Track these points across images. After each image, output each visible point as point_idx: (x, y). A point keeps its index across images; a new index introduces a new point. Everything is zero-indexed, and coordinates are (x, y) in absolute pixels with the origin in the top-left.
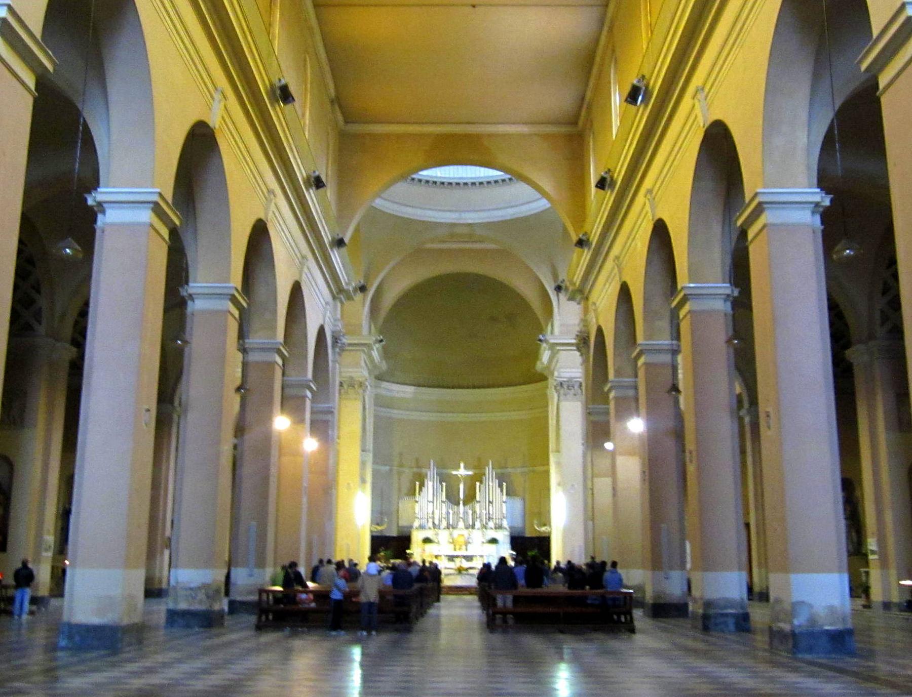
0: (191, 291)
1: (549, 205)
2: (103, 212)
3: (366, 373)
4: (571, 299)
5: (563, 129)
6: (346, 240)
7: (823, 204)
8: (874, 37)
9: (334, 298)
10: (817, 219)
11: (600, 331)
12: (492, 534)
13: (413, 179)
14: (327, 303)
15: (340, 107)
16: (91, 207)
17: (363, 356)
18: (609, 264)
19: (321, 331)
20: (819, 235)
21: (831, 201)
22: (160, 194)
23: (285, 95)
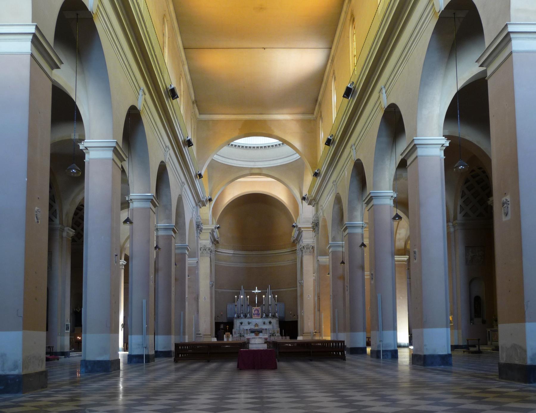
0: (131, 197)
2: (88, 153)
4: (310, 204)
6: (203, 174)
9: (197, 205)
10: (442, 154)
13: (232, 145)
14: (194, 207)
15: (197, 105)
16: (82, 150)
18: (330, 184)
21: (450, 144)
23: (173, 94)
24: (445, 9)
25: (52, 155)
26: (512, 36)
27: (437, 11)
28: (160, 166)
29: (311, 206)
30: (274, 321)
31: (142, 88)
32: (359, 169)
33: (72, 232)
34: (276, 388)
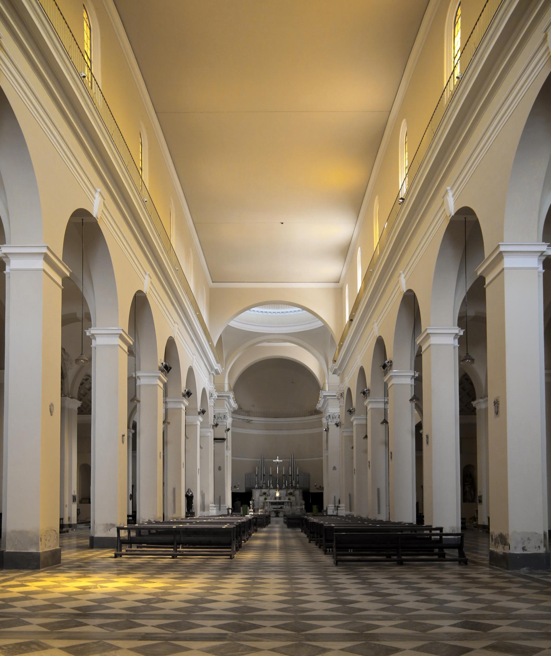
1: (323, 324)
2: (95, 339)
3: (227, 411)
5: (332, 285)
7: (460, 334)
8: (486, 258)
11: (349, 390)
12: (291, 491)
16: (89, 336)
17: (226, 402)
21: (464, 333)
22: (123, 330)
25: (62, 316)
26: (504, 254)
27: (448, 215)
28: (168, 340)
29: (335, 376)
30: (297, 492)
31: (148, 273)
32: (410, 302)
33: (78, 404)
34: (304, 569)
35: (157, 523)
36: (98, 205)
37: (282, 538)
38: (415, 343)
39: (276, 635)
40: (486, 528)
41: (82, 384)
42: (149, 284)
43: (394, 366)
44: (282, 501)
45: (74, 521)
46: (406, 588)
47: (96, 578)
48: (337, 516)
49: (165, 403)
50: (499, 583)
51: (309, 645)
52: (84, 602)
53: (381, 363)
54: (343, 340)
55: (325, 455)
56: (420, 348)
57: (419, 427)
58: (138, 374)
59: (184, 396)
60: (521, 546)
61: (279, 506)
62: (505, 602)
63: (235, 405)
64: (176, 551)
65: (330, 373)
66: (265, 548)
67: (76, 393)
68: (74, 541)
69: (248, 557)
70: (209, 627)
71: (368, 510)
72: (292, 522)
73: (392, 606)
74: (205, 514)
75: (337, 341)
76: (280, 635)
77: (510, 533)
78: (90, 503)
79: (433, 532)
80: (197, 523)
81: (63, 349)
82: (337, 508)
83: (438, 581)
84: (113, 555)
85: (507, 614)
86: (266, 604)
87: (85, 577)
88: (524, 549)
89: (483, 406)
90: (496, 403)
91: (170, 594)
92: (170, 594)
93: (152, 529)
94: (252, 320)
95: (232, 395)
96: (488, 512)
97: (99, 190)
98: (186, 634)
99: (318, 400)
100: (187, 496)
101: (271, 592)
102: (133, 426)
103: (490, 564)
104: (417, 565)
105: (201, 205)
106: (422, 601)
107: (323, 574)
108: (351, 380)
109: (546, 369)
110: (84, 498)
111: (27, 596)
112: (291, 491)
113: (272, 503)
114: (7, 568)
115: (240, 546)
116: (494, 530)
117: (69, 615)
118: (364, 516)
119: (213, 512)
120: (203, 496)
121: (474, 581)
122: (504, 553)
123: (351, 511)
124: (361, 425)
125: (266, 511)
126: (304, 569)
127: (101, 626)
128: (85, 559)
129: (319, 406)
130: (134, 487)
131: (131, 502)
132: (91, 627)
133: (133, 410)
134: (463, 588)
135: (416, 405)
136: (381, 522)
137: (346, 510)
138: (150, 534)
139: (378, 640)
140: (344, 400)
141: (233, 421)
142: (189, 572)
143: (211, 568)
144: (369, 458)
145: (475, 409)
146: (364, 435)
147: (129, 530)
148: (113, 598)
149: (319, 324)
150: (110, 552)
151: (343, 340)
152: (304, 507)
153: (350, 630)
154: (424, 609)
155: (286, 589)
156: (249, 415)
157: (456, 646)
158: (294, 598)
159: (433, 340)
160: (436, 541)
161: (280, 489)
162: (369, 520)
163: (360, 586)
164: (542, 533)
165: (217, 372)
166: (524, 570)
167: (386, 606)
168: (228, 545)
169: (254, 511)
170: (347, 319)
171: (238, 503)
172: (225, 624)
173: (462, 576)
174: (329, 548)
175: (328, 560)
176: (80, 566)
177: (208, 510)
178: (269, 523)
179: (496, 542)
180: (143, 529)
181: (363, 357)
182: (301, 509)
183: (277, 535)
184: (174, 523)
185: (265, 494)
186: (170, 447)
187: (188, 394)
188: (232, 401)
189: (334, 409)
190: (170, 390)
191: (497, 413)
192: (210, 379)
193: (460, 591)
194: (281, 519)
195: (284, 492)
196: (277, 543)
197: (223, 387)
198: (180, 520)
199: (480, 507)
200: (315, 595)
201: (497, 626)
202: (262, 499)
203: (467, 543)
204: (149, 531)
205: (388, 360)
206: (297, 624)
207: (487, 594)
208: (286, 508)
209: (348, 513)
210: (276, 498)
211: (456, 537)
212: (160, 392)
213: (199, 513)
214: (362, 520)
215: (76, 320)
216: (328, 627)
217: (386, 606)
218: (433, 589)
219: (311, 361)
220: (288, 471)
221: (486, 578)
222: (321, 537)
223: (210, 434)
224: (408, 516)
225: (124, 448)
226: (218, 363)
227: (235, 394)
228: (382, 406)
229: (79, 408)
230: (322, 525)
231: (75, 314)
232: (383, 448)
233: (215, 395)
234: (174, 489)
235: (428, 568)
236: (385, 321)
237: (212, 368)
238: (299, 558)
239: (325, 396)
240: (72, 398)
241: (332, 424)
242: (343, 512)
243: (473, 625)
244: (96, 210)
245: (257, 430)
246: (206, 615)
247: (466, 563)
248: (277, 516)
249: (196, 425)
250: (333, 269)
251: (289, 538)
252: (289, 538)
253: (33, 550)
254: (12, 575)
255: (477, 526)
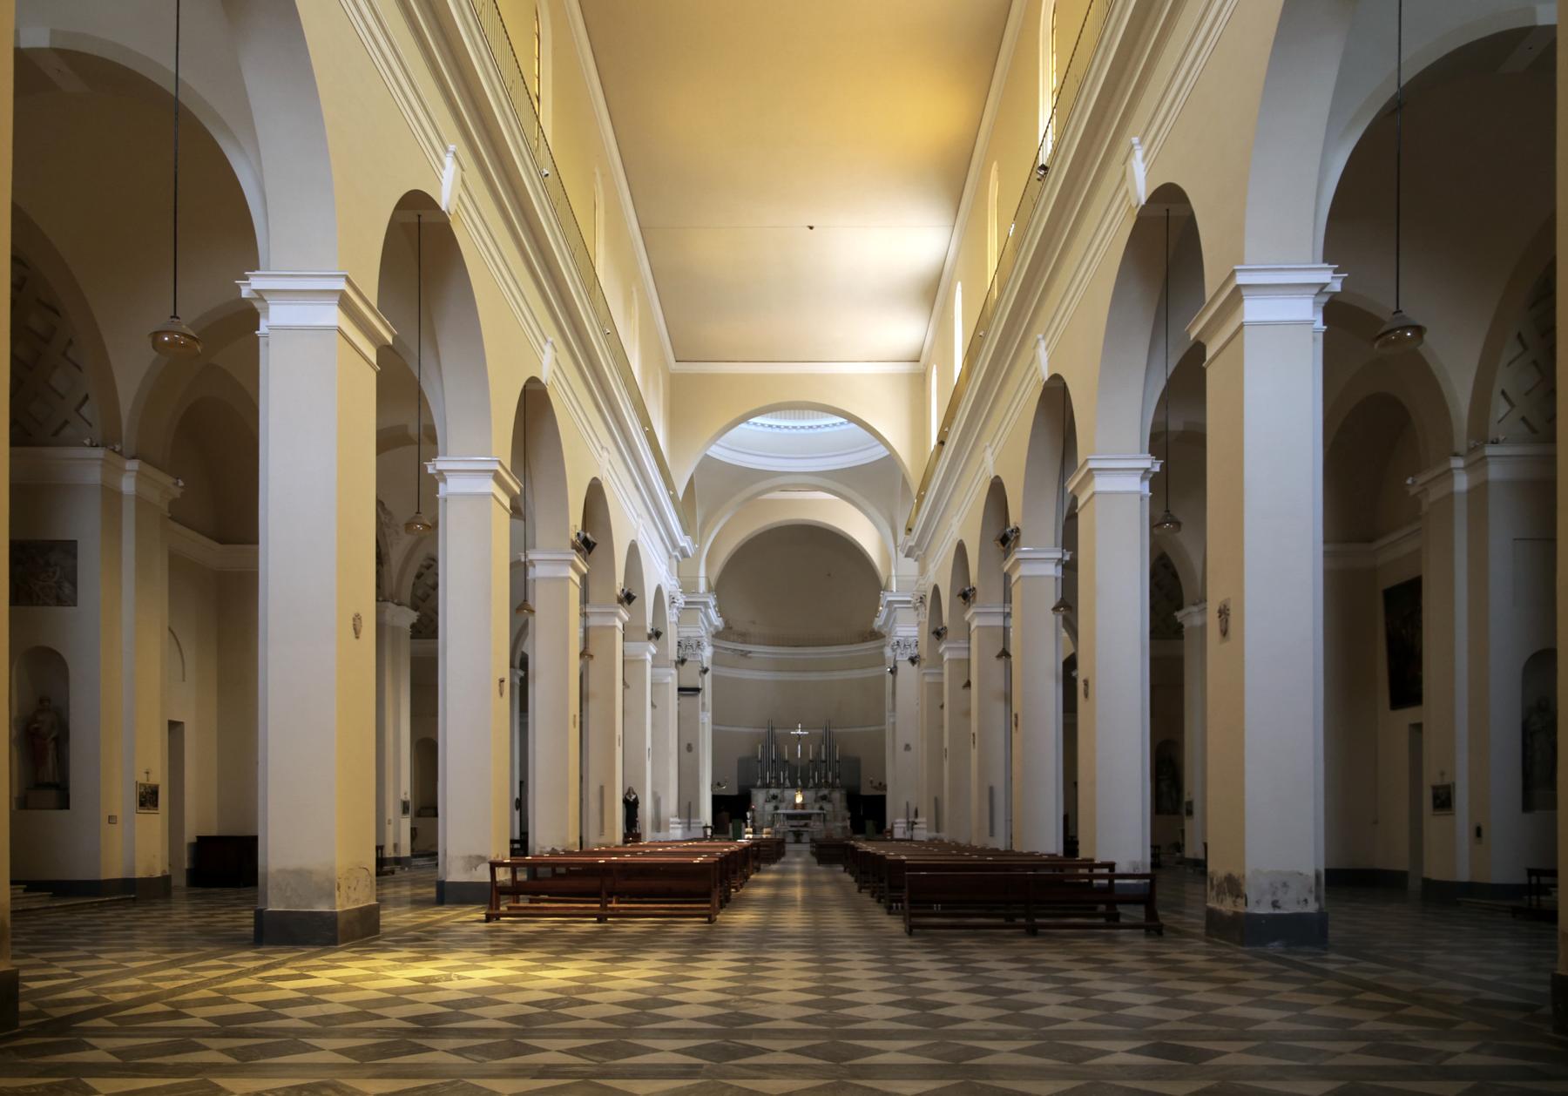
2: (445, 481)
5: (905, 368)
10: (1145, 489)
11: (936, 589)
12: (825, 792)
16: (431, 475)
19: (659, 590)
20: (1147, 501)
21: (1343, 284)
24: (1148, 202)
25: (379, 433)
28: (590, 486)
29: (910, 560)
30: (837, 795)
33: (413, 616)
34: (848, 942)
35: (569, 853)
36: (451, 183)
37: (807, 884)
38: (1064, 489)
39: (794, 1066)
40: (1200, 865)
41: (419, 576)
42: (550, 363)
43: (1022, 539)
44: (808, 811)
45: (406, 852)
46: (1042, 980)
47: (449, 960)
48: (911, 840)
49: (584, 615)
50: (1226, 971)
51: (857, 1086)
52: (425, 1005)
53: (995, 533)
54: (924, 486)
55: (889, 720)
56: (1075, 499)
57: (1070, 664)
58: (531, 556)
59: (620, 601)
60: (1269, 898)
61: (802, 822)
62: (1234, 1007)
63: (718, 622)
64: (607, 909)
65: (901, 555)
66: (776, 903)
67: (406, 595)
68: (406, 891)
69: (743, 918)
70: (667, 1052)
71: (970, 830)
72: (827, 852)
73: (1017, 1014)
74: (661, 836)
75: (915, 486)
76: (802, 1066)
77: (1248, 873)
78: (436, 815)
79: (1096, 871)
80: (645, 854)
81: (380, 503)
82: (911, 825)
83: (1104, 965)
84: (483, 917)
85: (1239, 1030)
86: (771, 1007)
87: (428, 959)
88: (1275, 904)
89: (1197, 621)
90: (1223, 613)
91: (592, 990)
92: (592, 990)
93: (559, 865)
94: (753, 443)
95: (712, 601)
96: (1204, 832)
97: (452, 147)
98: (624, 1066)
99: (877, 610)
100: (626, 801)
101: (787, 984)
102: (521, 663)
103: (1208, 934)
104: (1065, 936)
105: (660, 189)
106: (1073, 1004)
107: (885, 955)
108: (940, 570)
109: (1325, 542)
110: (425, 807)
111: (311, 997)
112: (825, 792)
113: (789, 817)
114: (271, 943)
115: (728, 899)
116: (1217, 867)
117: (397, 1030)
118: (963, 841)
119: (676, 832)
120: (657, 802)
121: (1175, 967)
122: (1236, 913)
123: (938, 831)
124: (959, 661)
125: (777, 832)
126: (848, 942)
127: (458, 1052)
128: (429, 924)
129: (878, 622)
130: (523, 784)
131: (517, 813)
132: (440, 1054)
133: (520, 633)
134: (1154, 980)
135: (1065, 619)
136: (995, 852)
137: (929, 830)
138: (555, 875)
139: (988, 1078)
140: (926, 611)
141: (715, 654)
142: (632, 948)
143: (672, 941)
144: (974, 727)
145: (1182, 626)
146: (964, 682)
147: (514, 867)
148: (482, 998)
149: (881, 452)
150: (476, 911)
151: (924, 486)
152: (848, 823)
153: (934, 1057)
154: (1076, 1019)
155: (815, 980)
156: (744, 642)
157: (1138, 1090)
158: (828, 997)
159: (1100, 484)
160: (1101, 889)
161: (804, 788)
162: (973, 850)
163: (955, 975)
164: (1312, 874)
165: (684, 554)
166: (1275, 947)
167: (1005, 1012)
168: (704, 896)
169: (754, 832)
170: (934, 441)
171: (725, 815)
172: (697, 1047)
173: (1152, 957)
174: (897, 901)
175: (895, 925)
176: (418, 939)
177: (667, 829)
178: (783, 854)
179: (1220, 893)
180: (541, 865)
181: (963, 521)
182: (844, 828)
183: (798, 877)
184: (601, 854)
185: (774, 797)
186: (593, 706)
187: (628, 598)
188: (712, 613)
189: (908, 629)
190: (594, 589)
191: (1224, 632)
192: (670, 567)
193: (1147, 986)
194: (806, 848)
195: (811, 794)
196: (798, 892)
197: (696, 584)
198: (612, 848)
199: (1188, 823)
200: (869, 992)
201: (1219, 1054)
202: (769, 807)
203: (1161, 895)
204: (554, 871)
205: (1012, 526)
206: (834, 1045)
207: (1201, 992)
208: (816, 826)
209: (933, 834)
210: (795, 806)
211: (1142, 881)
212: (575, 593)
213: (648, 835)
214: (959, 848)
215: (406, 441)
216: (892, 1053)
217: (1005, 1012)
218: (1096, 981)
219: (863, 531)
220: (819, 753)
221: (1198, 961)
222: (881, 881)
223: (671, 678)
224: (1049, 842)
225: (502, 706)
226: (686, 533)
227: (718, 599)
228: (998, 621)
229: (413, 626)
230: (883, 857)
231: (405, 427)
232: (1000, 706)
233: (681, 600)
234: (602, 788)
235: (1084, 942)
236: (1006, 446)
237: (674, 544)
238: (839, 921)
239: (890, 603)
240: (399, 604)
241: (903, 660)
242: (922, 833)
243: (1172, 1051)
244: (446, 196)
245: (761, 671)
246: (663, 1030)
247: (1160, 933)
248: (798, 841)
249: (644, 661)
250: (905, 331)
251: (820, 883)
252: (820, 883)
253: (323, 908)
254: (281, 957)
255: (1183, 862)
